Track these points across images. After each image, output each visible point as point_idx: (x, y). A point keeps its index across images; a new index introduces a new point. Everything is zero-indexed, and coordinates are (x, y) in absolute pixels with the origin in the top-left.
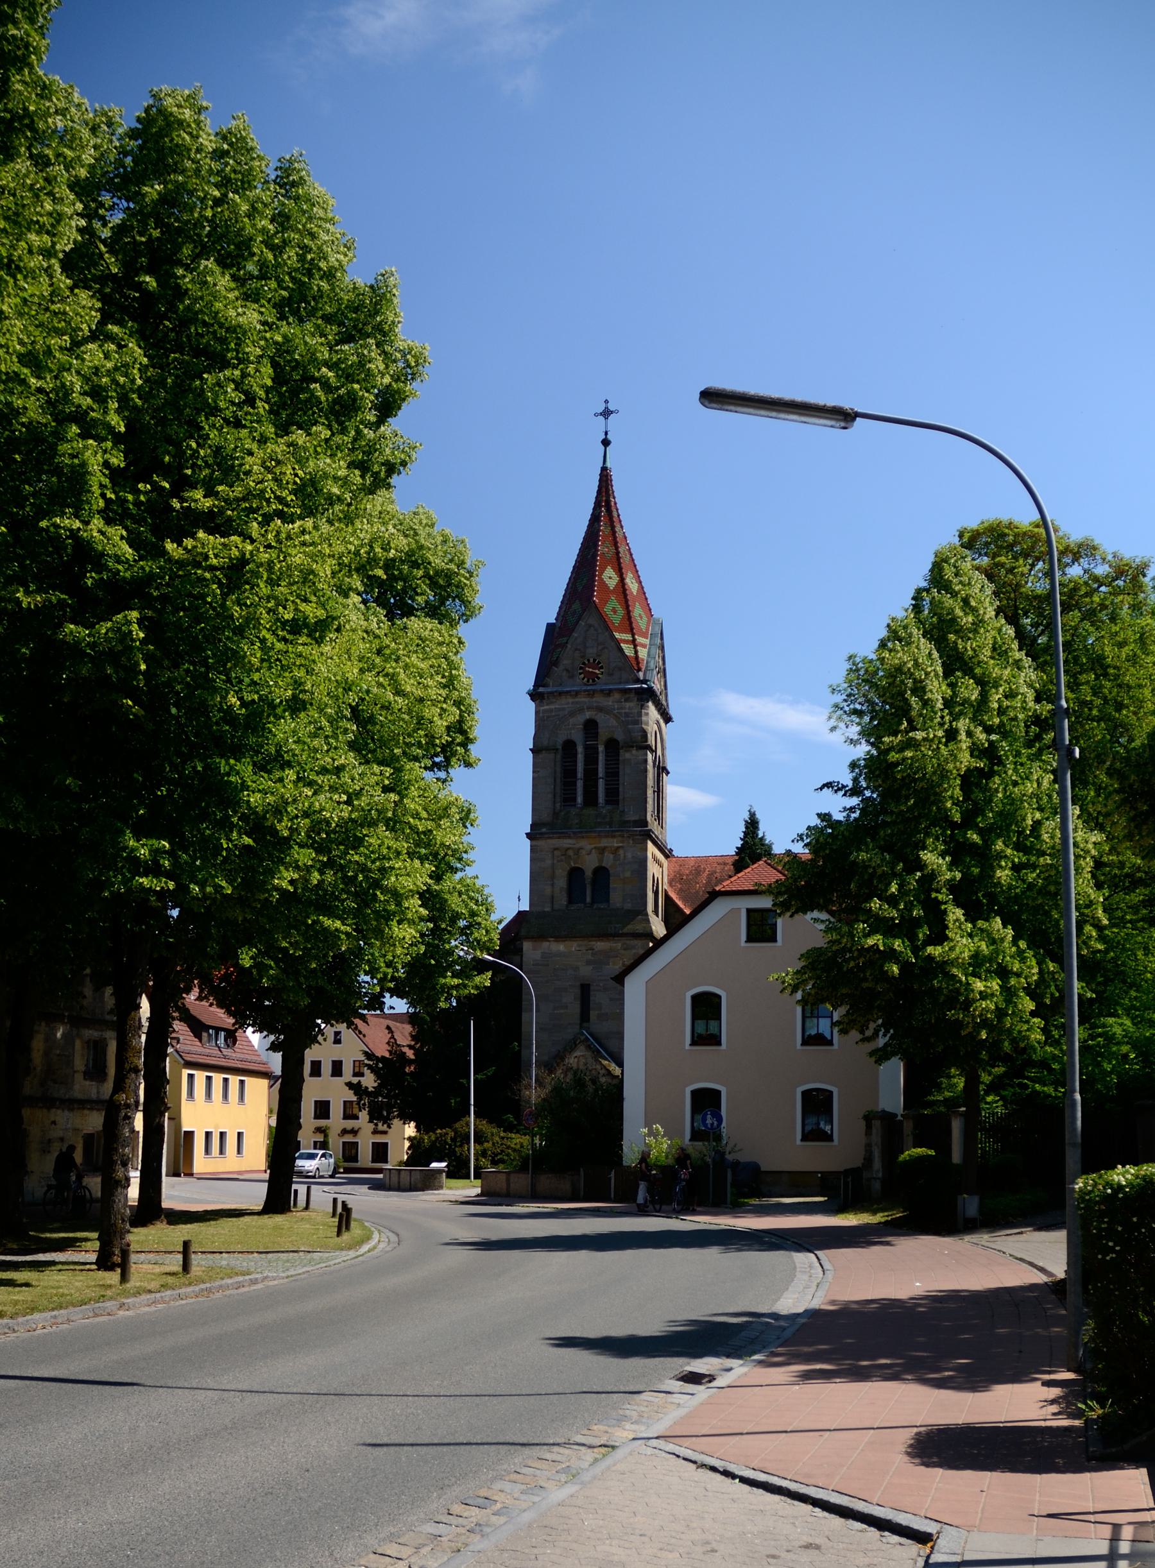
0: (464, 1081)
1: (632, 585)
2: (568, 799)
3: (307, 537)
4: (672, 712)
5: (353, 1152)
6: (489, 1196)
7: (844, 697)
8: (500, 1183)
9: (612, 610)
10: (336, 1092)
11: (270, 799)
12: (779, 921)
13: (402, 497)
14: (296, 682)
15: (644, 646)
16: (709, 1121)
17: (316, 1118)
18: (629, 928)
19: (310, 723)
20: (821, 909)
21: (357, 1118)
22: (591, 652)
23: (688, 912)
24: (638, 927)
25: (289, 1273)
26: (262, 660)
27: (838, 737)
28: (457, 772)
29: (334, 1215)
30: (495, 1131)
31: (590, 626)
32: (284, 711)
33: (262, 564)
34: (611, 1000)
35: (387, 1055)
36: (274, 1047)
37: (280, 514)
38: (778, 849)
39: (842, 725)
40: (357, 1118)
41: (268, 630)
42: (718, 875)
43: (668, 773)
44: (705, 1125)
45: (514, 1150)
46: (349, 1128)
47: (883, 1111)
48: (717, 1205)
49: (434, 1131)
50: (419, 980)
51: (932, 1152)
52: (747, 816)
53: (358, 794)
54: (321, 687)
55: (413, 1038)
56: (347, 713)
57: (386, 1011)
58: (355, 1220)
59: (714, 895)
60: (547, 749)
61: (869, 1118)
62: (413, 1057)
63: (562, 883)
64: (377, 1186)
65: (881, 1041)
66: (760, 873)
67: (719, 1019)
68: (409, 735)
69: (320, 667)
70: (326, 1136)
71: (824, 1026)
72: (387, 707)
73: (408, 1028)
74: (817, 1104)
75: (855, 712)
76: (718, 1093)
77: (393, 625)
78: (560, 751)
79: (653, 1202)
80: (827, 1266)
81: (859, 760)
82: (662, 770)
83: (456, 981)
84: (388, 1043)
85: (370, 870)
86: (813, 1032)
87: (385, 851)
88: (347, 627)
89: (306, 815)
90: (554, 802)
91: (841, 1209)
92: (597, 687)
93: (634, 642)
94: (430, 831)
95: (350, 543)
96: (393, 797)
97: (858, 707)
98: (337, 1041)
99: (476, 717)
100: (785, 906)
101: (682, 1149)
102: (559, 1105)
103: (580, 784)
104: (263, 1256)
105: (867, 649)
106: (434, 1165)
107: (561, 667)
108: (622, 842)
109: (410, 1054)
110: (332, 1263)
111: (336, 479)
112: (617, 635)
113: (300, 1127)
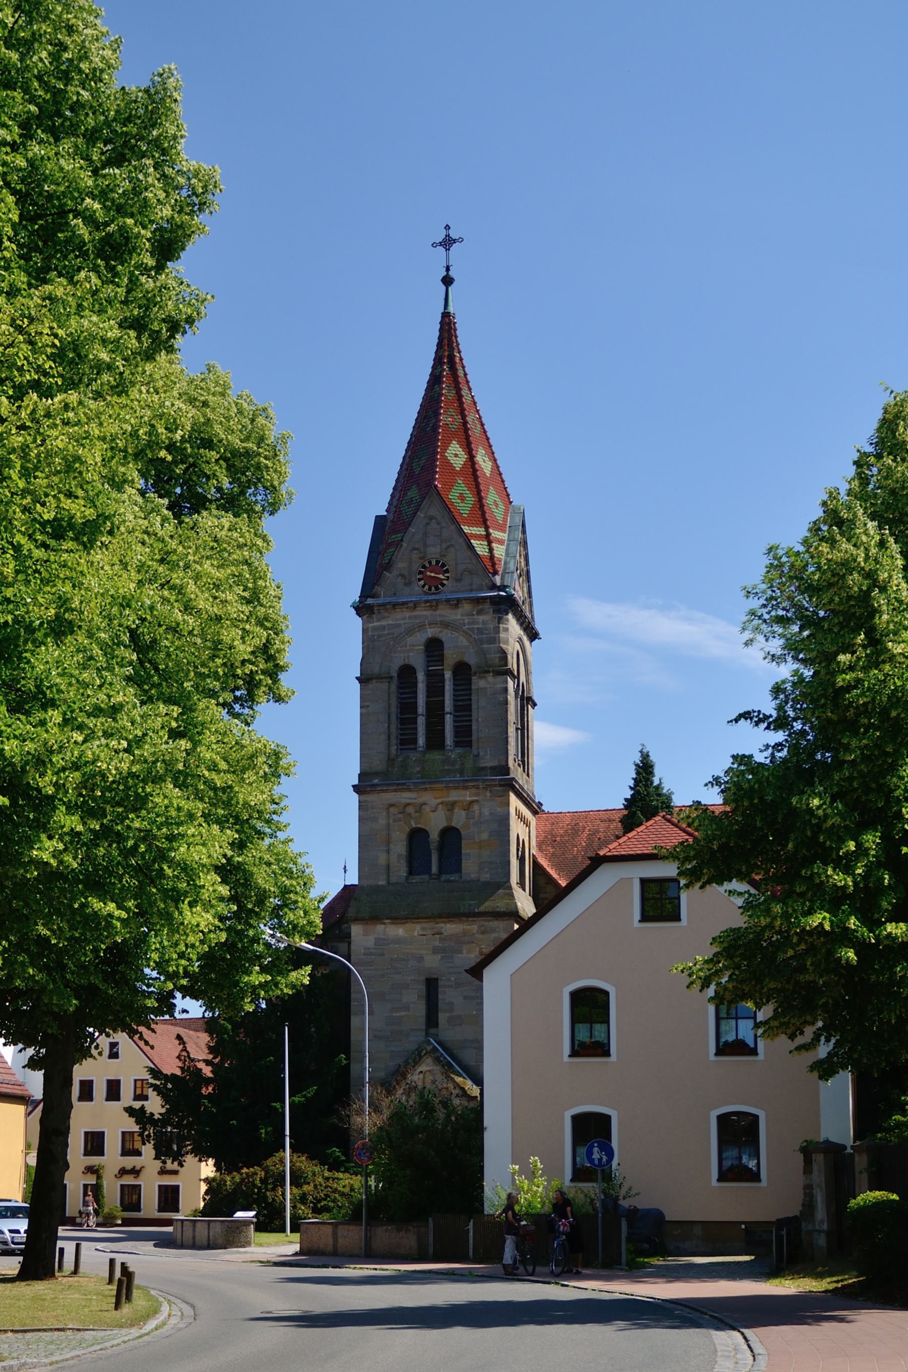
0: (278, 1105)
1: (484, 464)
2: (407, 741)
3: (71, 414)
4: (538, 626)
5: (135, 1197)
6: (311, 1255)
7: (762, 601)
8: (324, 1238)
9: (459, 496)
10: (113, 1120)
11: (30, 746)
12: (684, 896)
13: (188, 357)
14: (60, 598)
15: (501, 542)
16: (596, 1156)
17: (86, 1154)
18: (487, 906)
19: (78, 651)
20: (742, 877)
21: (139, 1154)
22: (433, 552)
23: (563, 883)
24: (497, 903)
25: (54, 1359)
26: (17, 572)
27: (755, 654)
28: (265, 709)
29: (110, 1281)
30: (317, 1169)
31: (431, 518)
32: (46, 635)
33: (13, 451)
34: (465, 998)
35: (178, 1072)
36: (33, 1064)
37: (36, 385)
38: (679, 800)
39: (760, 638)
40: (139, 1154)
41: (24, 534)
42: (601, 835)
43: (534, 705)
44: (591, 1161)
45: (342, 1194)
46: (129, 1167)
47: (827, 1142)
48: (611, 1265)
49: (238, 1170)
50: (216, 975)
51: (895, 1197)
52: (637, 759)
53: (139, 741)
54: (92, 604)
55: (211, 1050)
56: (126, 638)
57: (177, 1015)
58: (139, 1288)
59: (597, 862)
60: (379, 678)
61: (808, 1150)
62: (211, 1075)
63: (400, 848)
64: (165, 1242)
65: (823, 1050)
66: (654, 834)
67: (607, 1022)
68: (203, 665)
69: (91, 581)
70: (99, 1177)
71: (745, 1030)
72: (174, 629)
73: (204, 1038)
74: (738, 1131)
75: (780, 620)
76: (608, 1118)
77: (181, 523)
78: (395, 681)
79: (524, 1262)
80: (758, 1349)
81: (784, 682)
82: (526, 701)
83: (263, 978)
84: (179, 1057)
85: (155, 837)
86: (731, 1038)
87: (173, 813)
88: (122, 529)
89: (76, 767)
90: (389, 746)
91: (774, 1273)
92: (442, 597)
93: (488, 537)
94: (231, 787)
95: (126, 422)
96: (184, 744)
97: (781, 613)
98: (114, 1055)
99: (286, 636)
100: (694, 876)
101: (561, 1192)
102: (400, 1133)
103: (421, 721)
104: (20, 1335)
105: (792, 535)
106: (239, 1214)
107: (395, 573)
108: (477, 795)
109: (207, 1071)
110: (108, 1344)
111: (104, 341)
112: (466, 529)
113: (67, 1166)
